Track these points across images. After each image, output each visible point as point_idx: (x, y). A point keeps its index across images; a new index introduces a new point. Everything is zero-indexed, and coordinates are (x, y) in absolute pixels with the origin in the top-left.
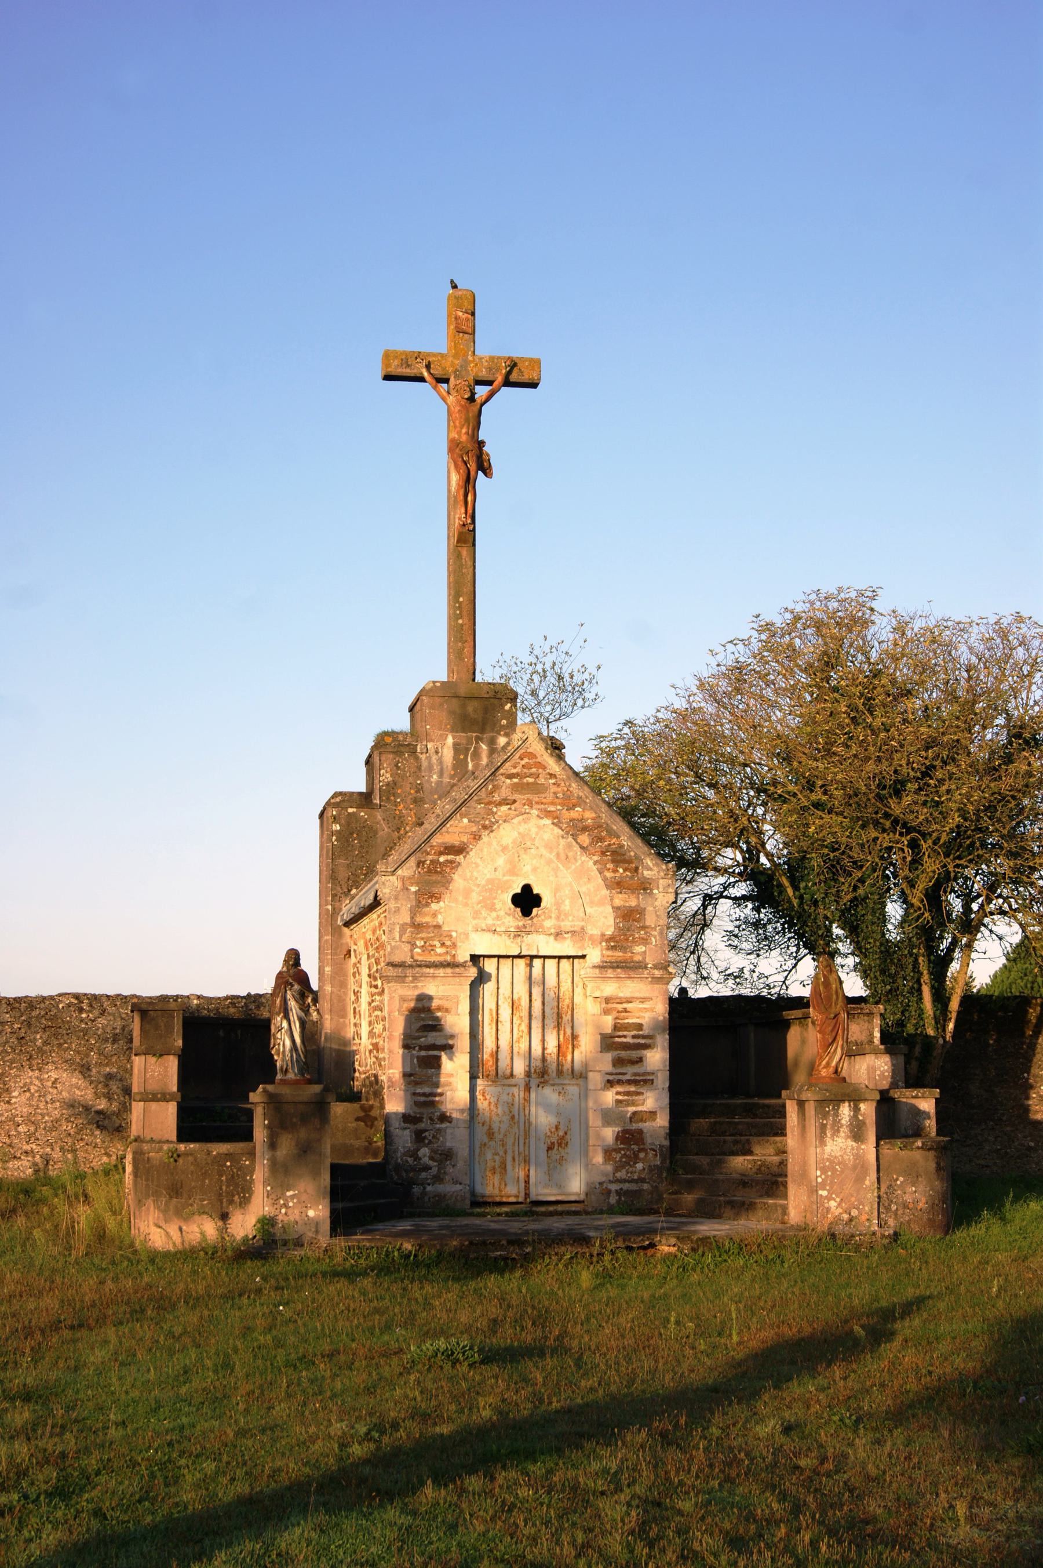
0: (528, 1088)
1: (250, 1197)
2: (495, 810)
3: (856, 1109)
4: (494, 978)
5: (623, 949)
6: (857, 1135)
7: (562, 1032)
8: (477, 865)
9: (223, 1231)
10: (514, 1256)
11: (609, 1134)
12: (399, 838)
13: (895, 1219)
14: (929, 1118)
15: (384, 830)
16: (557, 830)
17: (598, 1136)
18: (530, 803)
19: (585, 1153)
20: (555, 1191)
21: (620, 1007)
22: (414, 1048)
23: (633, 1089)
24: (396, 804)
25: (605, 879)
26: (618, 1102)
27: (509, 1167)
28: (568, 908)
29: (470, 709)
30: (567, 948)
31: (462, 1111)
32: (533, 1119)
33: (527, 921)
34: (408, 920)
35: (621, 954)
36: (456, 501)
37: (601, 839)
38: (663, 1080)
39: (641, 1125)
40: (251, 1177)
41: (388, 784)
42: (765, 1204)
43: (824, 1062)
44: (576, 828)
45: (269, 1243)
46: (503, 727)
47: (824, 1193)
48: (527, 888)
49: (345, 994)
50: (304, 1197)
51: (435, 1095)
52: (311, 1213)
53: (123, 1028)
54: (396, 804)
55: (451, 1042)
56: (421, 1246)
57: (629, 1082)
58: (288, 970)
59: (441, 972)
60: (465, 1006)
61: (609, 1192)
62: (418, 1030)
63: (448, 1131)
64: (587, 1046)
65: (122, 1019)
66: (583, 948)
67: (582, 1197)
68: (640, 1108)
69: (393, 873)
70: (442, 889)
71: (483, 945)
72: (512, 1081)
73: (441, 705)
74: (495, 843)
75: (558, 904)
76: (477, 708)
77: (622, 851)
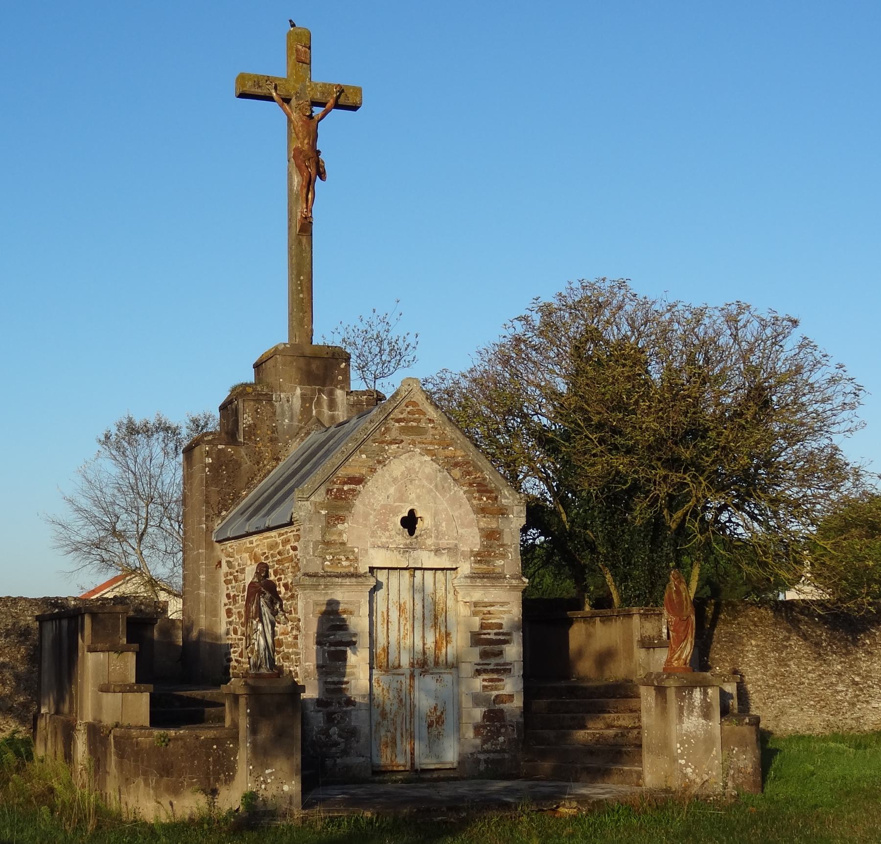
0: (412, 676)
1: (234, 776)
2: (387, 448)
3: (705, 694)
4: (385, 586)
5: (487, 562)
6: (706, 715)
7: (438, 631)
8: (374, 494)
9: (212, 804)
10: (452, 820)
11: (478, 713)
12: (259, 470)
13: (733, 781)
14: (732, 698)
15: (247, 463)
16: (435, 466)
17: (469, 716)
18: (414, 443)
19: (458, 728)
20: (434, 761)
21: (485, 610)
22: (325, 645)
23: (495, 676)
24: (256, 442)
25: (472, 506)
26: (485, 687)
27: (398, 742)
28: (444, 529)
29: (314, 366)
30: (444, 562)
31: (364, 696)
32: (416, 702)
33: (413, 539)
34: (320, 538)
35: (485, 567)
36: (297, 199)
37: (469, 473)
38: (518, 670)
39: (502, 706)
40: (235, 758)
41: (250, 426)
42: (620, 770)
43: (676, 656)
44: (451, 464)
45: (255, 815)
46: (340, 382)
47: (683, 762)
48: (412, 512)
49: (217, 597)
50: (280, 774)
51: (343, 683)
52: (286, 788)
53: (14, 624)
54: (256, 442)
55: (354, 639)
56: (378, 814)
57: (493, 671)
58: (260, 581)
59: (347, 581)
60: (365, 610)
61: (478, 761)
62: (328, 630)
63: (353, 713)
64: (459, 642)
65: (13, 617)
66: (456, 561)
67: (455, 765)
68: (501, 692)
69: (307, 499)
70: (346, 513)
71: (379, 558)
72: (400, 671)
73: (291, 362)
74: (387, 475)
75: (437, 526)
76: (323, 367)
77: (485, 483)
